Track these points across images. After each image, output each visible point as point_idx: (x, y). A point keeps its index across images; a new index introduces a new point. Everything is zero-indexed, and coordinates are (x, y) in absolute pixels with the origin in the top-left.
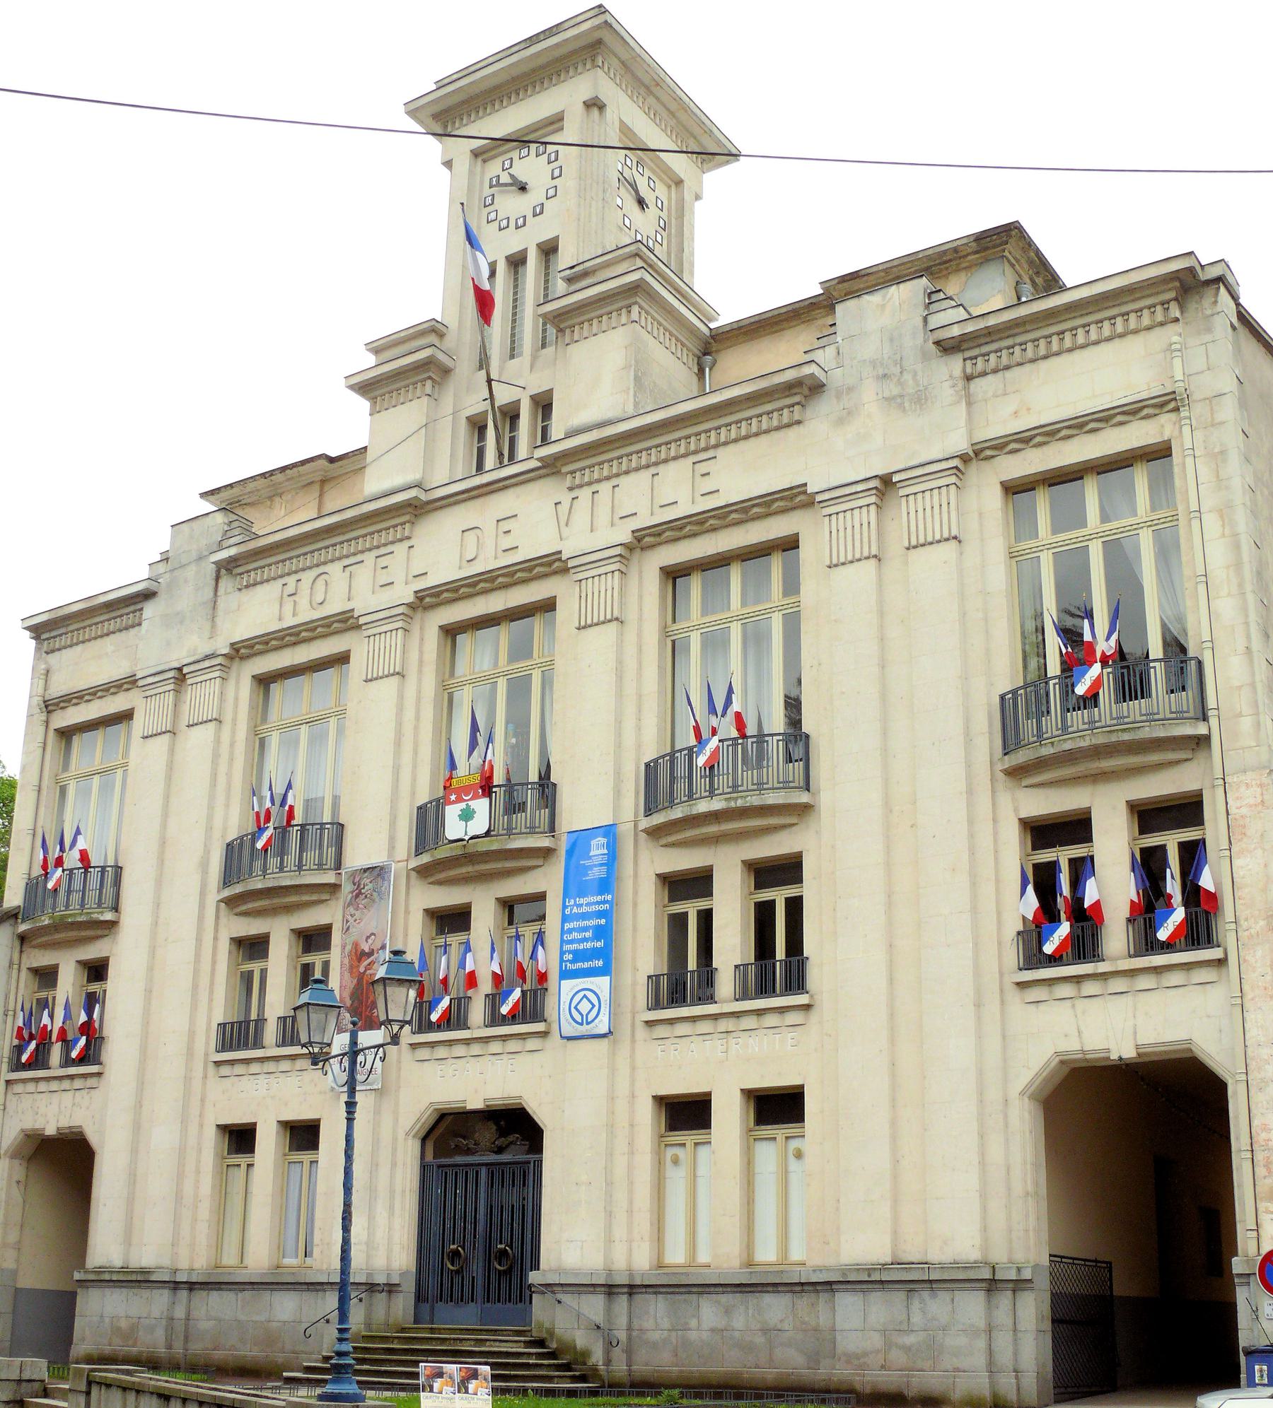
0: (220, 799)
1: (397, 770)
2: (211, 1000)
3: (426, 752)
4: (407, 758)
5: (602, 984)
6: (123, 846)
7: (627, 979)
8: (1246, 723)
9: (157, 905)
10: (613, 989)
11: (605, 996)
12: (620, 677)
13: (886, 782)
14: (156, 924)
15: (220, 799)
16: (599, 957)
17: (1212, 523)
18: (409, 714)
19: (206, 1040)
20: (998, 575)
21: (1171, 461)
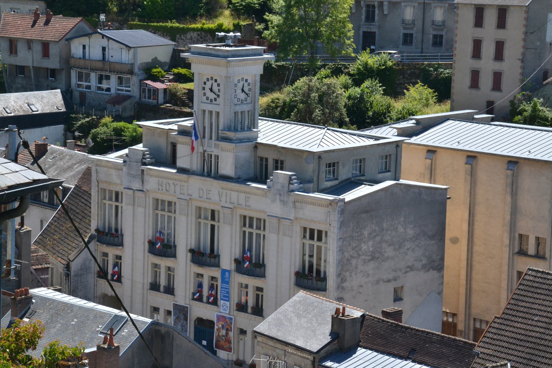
0: (147, 217)
1: (187, 238)
2: (147, 276)
3: (193, 236)
4: (189, 237)
5: (228, 303)
6: (176, 242)
7: (232, 303)
8: (332, 293)
9: (133, 248)
10: (230, 304)
11: (228, 306)
12: (232, 237)
13: (277, 281)
14: (133, 253)
15: (147, 217)
16: (227, 298)
17: (331, 251)
18: (189, 226)
19: (147, 286)
20: (298, 246)
21: (524, 235)
